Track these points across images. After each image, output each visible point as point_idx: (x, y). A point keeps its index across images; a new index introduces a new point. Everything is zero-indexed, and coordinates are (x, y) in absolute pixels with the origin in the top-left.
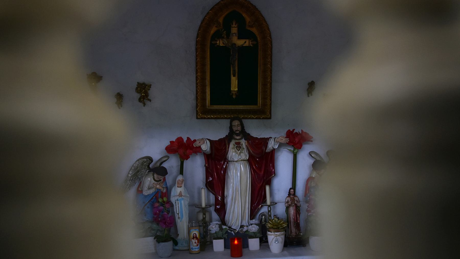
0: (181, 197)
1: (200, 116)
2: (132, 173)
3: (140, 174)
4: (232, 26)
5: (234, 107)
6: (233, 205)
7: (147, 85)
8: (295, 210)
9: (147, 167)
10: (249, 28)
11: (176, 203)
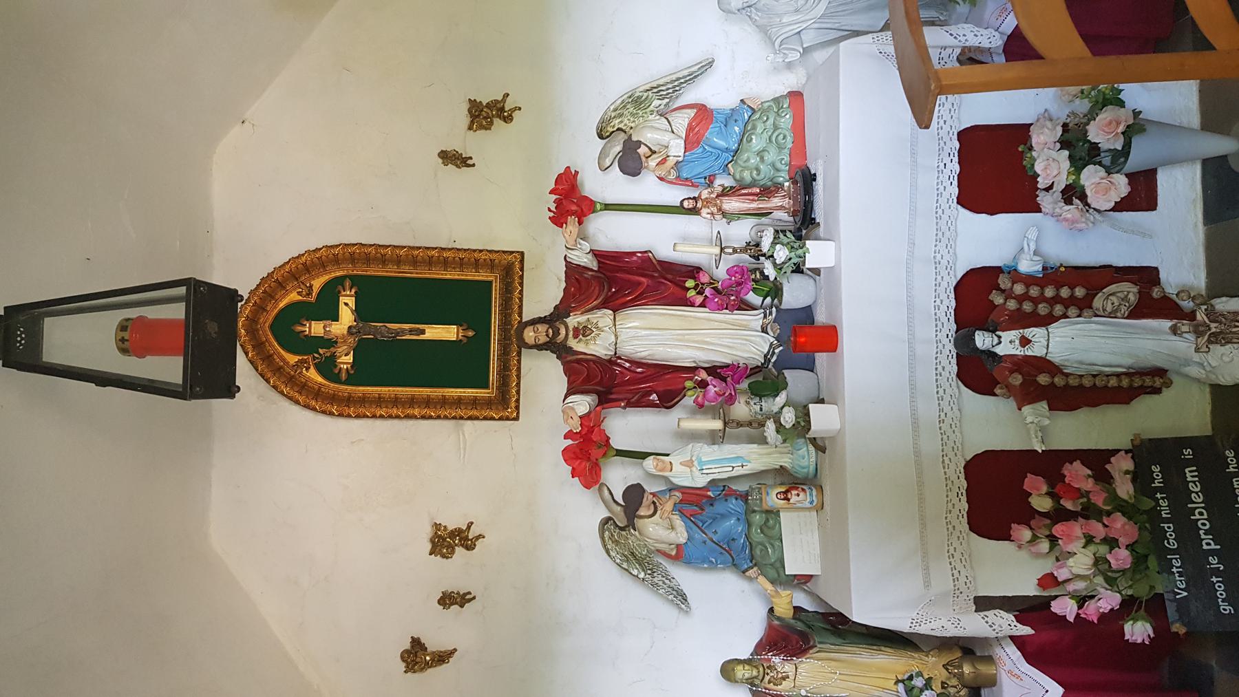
0: (693, 462)
1: (512, 412)
2: (637, 569)
4: (307, 333)
6: (713, 348)
7: (436, 533)
8: (730, 198)
9: (624, 533)
11: (707, 474)
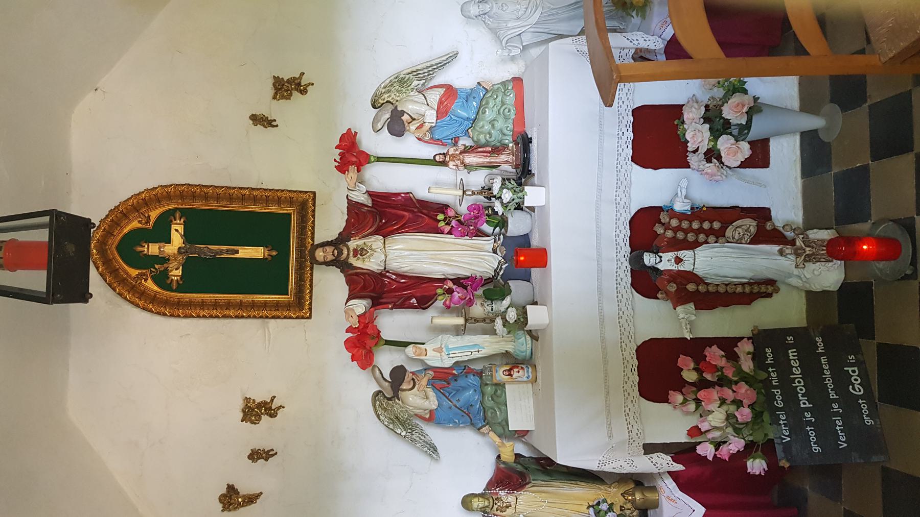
1: (306, 313)
3: (402, 415)
5: (293, 254)
9: (391, 402)
10: (151, 223)
11: (453, 357)
